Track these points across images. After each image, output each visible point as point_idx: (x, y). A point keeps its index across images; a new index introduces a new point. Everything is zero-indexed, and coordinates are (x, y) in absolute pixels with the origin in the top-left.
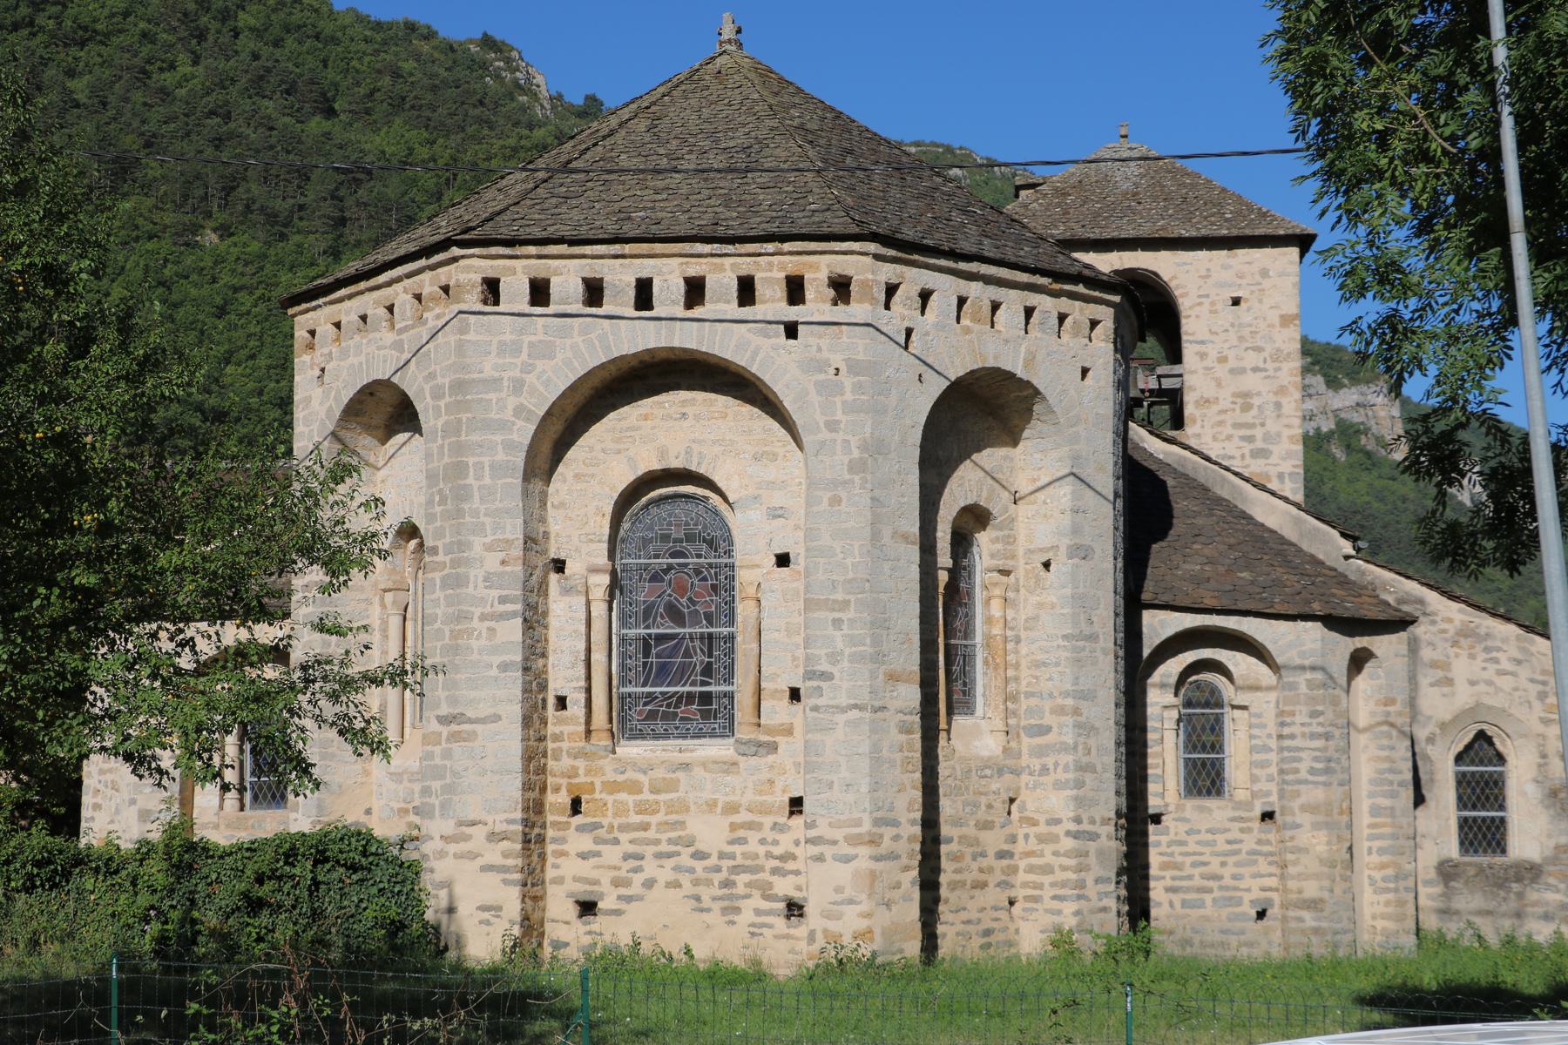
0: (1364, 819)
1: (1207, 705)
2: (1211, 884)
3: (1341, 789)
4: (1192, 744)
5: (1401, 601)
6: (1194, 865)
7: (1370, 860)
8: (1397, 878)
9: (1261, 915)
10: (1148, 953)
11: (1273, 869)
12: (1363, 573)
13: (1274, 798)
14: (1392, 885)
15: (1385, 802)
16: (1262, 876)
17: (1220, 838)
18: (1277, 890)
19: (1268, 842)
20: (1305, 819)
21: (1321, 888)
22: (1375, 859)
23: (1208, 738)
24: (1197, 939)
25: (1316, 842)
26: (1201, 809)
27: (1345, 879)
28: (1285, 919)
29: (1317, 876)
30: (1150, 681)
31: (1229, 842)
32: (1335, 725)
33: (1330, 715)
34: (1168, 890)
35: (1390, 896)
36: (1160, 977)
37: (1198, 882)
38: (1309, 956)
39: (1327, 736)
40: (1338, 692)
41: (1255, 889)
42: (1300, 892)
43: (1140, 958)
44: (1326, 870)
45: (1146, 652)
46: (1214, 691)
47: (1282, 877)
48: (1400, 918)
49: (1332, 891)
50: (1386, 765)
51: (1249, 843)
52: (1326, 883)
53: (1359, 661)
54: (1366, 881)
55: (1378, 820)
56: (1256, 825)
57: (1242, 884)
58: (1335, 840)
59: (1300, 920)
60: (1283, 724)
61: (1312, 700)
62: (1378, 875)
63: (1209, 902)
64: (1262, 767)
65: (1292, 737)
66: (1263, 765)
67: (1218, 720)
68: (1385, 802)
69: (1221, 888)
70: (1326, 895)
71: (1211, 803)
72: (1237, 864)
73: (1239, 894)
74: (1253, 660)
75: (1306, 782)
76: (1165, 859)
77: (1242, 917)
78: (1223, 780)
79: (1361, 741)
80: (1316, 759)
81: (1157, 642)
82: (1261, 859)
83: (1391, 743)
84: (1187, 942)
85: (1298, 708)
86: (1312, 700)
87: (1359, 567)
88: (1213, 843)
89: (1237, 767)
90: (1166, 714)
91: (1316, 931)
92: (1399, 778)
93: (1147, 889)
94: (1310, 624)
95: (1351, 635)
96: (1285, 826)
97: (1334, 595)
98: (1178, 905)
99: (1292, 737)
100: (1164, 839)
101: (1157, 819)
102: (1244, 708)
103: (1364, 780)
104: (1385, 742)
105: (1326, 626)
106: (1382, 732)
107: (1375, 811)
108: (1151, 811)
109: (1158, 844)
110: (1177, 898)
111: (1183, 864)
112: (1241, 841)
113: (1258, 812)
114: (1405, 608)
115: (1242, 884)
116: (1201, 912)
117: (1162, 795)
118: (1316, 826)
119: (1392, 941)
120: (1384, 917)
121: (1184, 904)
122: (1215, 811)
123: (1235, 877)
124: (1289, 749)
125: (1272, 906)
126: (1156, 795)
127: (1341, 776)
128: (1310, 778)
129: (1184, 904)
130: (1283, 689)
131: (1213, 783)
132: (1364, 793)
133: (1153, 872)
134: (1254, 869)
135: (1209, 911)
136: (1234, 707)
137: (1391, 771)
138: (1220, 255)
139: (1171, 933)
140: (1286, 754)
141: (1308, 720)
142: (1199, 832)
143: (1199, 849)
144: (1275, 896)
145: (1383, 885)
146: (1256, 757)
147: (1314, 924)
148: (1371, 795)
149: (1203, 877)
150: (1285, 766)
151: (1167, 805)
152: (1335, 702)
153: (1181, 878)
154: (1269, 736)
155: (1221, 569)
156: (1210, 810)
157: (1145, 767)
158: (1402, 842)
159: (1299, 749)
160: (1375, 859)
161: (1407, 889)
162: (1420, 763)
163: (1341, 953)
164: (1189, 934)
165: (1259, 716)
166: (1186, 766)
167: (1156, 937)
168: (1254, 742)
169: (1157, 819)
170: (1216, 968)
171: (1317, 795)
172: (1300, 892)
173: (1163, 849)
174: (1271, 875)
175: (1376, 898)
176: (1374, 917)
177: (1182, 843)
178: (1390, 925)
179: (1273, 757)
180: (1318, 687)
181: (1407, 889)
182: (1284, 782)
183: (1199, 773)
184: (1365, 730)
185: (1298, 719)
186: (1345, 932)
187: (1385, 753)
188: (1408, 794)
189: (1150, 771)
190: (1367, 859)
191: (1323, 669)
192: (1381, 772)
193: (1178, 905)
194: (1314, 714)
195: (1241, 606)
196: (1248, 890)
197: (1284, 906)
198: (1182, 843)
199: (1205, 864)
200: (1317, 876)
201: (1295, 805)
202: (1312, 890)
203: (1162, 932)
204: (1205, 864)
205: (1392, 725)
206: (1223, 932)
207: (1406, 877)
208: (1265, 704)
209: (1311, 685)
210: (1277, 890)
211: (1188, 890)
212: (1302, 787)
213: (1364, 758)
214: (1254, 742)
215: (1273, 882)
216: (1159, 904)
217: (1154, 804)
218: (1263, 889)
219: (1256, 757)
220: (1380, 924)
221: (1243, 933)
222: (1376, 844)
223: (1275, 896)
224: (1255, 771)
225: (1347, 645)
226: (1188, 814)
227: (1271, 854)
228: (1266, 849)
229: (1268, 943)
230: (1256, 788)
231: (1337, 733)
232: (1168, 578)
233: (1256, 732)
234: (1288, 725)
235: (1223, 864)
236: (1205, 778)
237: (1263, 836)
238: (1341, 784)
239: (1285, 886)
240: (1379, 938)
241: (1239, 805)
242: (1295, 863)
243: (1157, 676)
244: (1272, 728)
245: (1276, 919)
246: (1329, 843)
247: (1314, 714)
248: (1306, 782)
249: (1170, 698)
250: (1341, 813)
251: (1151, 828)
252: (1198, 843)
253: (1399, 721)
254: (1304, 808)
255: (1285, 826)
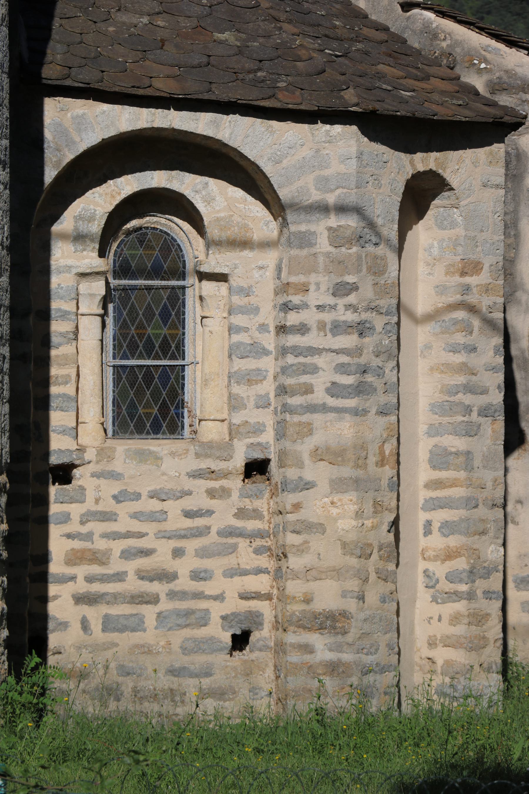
0: (420, 473)
1: (156, 272)
2: (155, 587)
3: (383, 421)
4: (128, 342)
5: (497, 87)
6: (127, 555)
7: (427, 545)
8: (472, 574)
9: (240, 641)
10: (40, 712)
11: (264, 561)
12: (434, 35)
13: (268, 437)
14: (463, 588)
15: (456, 443)
16: (244, 573)
17: (174, 508)
18: (268, 597)
19: (256, 514)
20: (319, 473)
21: (344, 595)
22: (436, 542)
23: (156, 331)
24: (128, 685)
25: (338, 513)
26: (142, 456)
27: (385, 577)
28: (280, 648)
29: (337, 573)
30: (56, 228)
31: (188, 514)
32: (375, 309)
33: (367, 291)
34: (80, 599)
35: (461, 606)
36: (61, 756)
37: (132, 585)
38: (320, 712)
39: (362, 329)
40: (381, 250)
41: (232, 596)
42: (308, 600)
43: (26, 722)
44: (353, 561)
45: (50, 175)
46: (170, 246)
47: (278, 575)
48: (476, 645)
49: (361, 598)
50: (461, 379)
51: (224, 516)
52: (353, 585)
53: (420, 195)
54: (421, 579)
55: (443, 474)
56: (236, 483)
57: (210, 588)
58: (369, 508)
59: (308, 649)
60: (286, 307)
61: (339, 264)
62: (440, 570)
63: (150, 621)
64: (250, 382)
65: (302, 329)
66: (251, 378)
67: (177, 298)
68: (456, 443)
69: (172, 595)
70: (351, 605)
71: (160, 446)
72: (203, 553)
73: (203, 605)
74: (238, 193)
75: (324, 408)
76: (77, 544)
77: (206, 645)
78: (181, 404)
79: (419, 338)
80: (342, 369)
81: (70, 156)
82: (243, 544)
83: (469, 340)
84: (110, 692)
85: (313, 278)
86: (339, 264)
87: (427, 28)
88: (159, 517)
89: (206, 382)
90: (84, 287)
91: (333, 668)
92: (482, 400)
93: (44, 599)
94: (338, 129)
95: (409, 149)
96: (286, 486)
97: (381, 76)
98: (96, 626)
99: (302, 329)
100: (76, 510)
101: (64, 474)
102: (222, 278)
103: (423, 404)
104: (460, 338)
105: (365, 133)
106: (456, 322)
107: (440, 459)
108: (54, 460)
109: (66, 518)
110: (94, 614)
111: (108, 553)
112: (210, 513)
113: (239, 463)
114: (505, 100)
115: (210, 588)
116: (137, 637)
117: (75, 432)
118: (338, 485)
119: (461, 683)
120: (449, 642)
121: (109, 624)
122: (168, 459)
123: (197, 576)
124: (297, 351)
125: (260, 625)
126: (64, 432)
127: (383, 399)
128: (331, 402)
129: (109, 624)
130: (289, 244)
131: (164, 410)
132: (422, 428)
133: (55, 567)
134: (230, 561)
135: (150, 635)
136: (203, 276)
137: (469, 389)
138: (302, 130)
139: (83, 675)
140: (290, 359)
141: (330, 300)
142: (137, 496)
143: (136, 526)
144: (265, 608)
145: (449, 587)
146: (240, 364)
147: (330, 656)
148: (434, 431)
149: (142, 575)
150: (290, 381)
151: (81, 450)
152: (377, 269)
153: (104, 579)
154: (263, 328)
155: (185, 24)
156: (157, 459)
157: (45, 382)
158: (482, 511)
159: (312, 351)
160: (436, 542)
161: (488, 594)
162: (518, 375)
163: (374, 706)
164: (113, 676)
165: (246, 292)
166: (117, 381)
167: (56, 684)
168: (236, 338)
169: (64, 474)
170: (157, 737)
171: (342, 431)
172: (308, 600)
173: (74, 527)
174: (259, 571)
175: (436, 609)
176: (432, 644)
177: (107, 517)
178: (459, 657)
179: (269, 364)
180: (350, 242)
181: (488, 594)
182: (286, 408)
183: (140, 393)
184: (429, 318)
185: (314, 298)
186: (383, 670)
187: (459, 358)
188: (494, 430)
189: (54, 390)
190: (423, 542)
191: (358, 211)
192: (453, 391)
193: (96, 626)
194: (341, 290)
195: (219, 94)
196: (220, 598)
197: (280, 625)
198: (107, 517)
199: (146, 553)
200: (337, 573)
201: (304, 448)
202: (328, 596)
203: (67, 675)
204: (146, 553)
205: (472, 309)
206: (173, 672)
207: (487, 574)
208: (256, 271)
209: (336, 237)
210: (268, 597)
211: (115, 599)
212: (317, 419)
213: (422, 365)
214: (236, 338)
215: (262, 583)
216: (64, 625)
217: (60, 446)
218: (245, 597)
219: (240, 364)
220: (442, 655)
221: (208, 674)
222: (440, 516)
223: (265, 608)
224: (237, 389)
225: (401, 166)
226: (118, 466)
227: (261, 534)
228: (252, 525)
229: (252, 690)
230: (237, 419)
231: (379, 322)
232: (89, 38)
233: (239, 320)
234: (297, 308)
235: (178, 553)
236: (150, 402)
237: (247, 504)
238: (382, 413)
239: (282, 590)
240: (437, 680)
241: (208, 449)
242: (301, 549)
243: (66, 223)
244: (268, 315)
245: (265, 648)
246: (359, 515)
247: (341, 290)
248: (324, 408)
249: (90, 259)
250: (381, 463)
251: (54, 490)
252: (136, 516)
253: (485, 302)
254: (318, 455)
255: (286, 486)
